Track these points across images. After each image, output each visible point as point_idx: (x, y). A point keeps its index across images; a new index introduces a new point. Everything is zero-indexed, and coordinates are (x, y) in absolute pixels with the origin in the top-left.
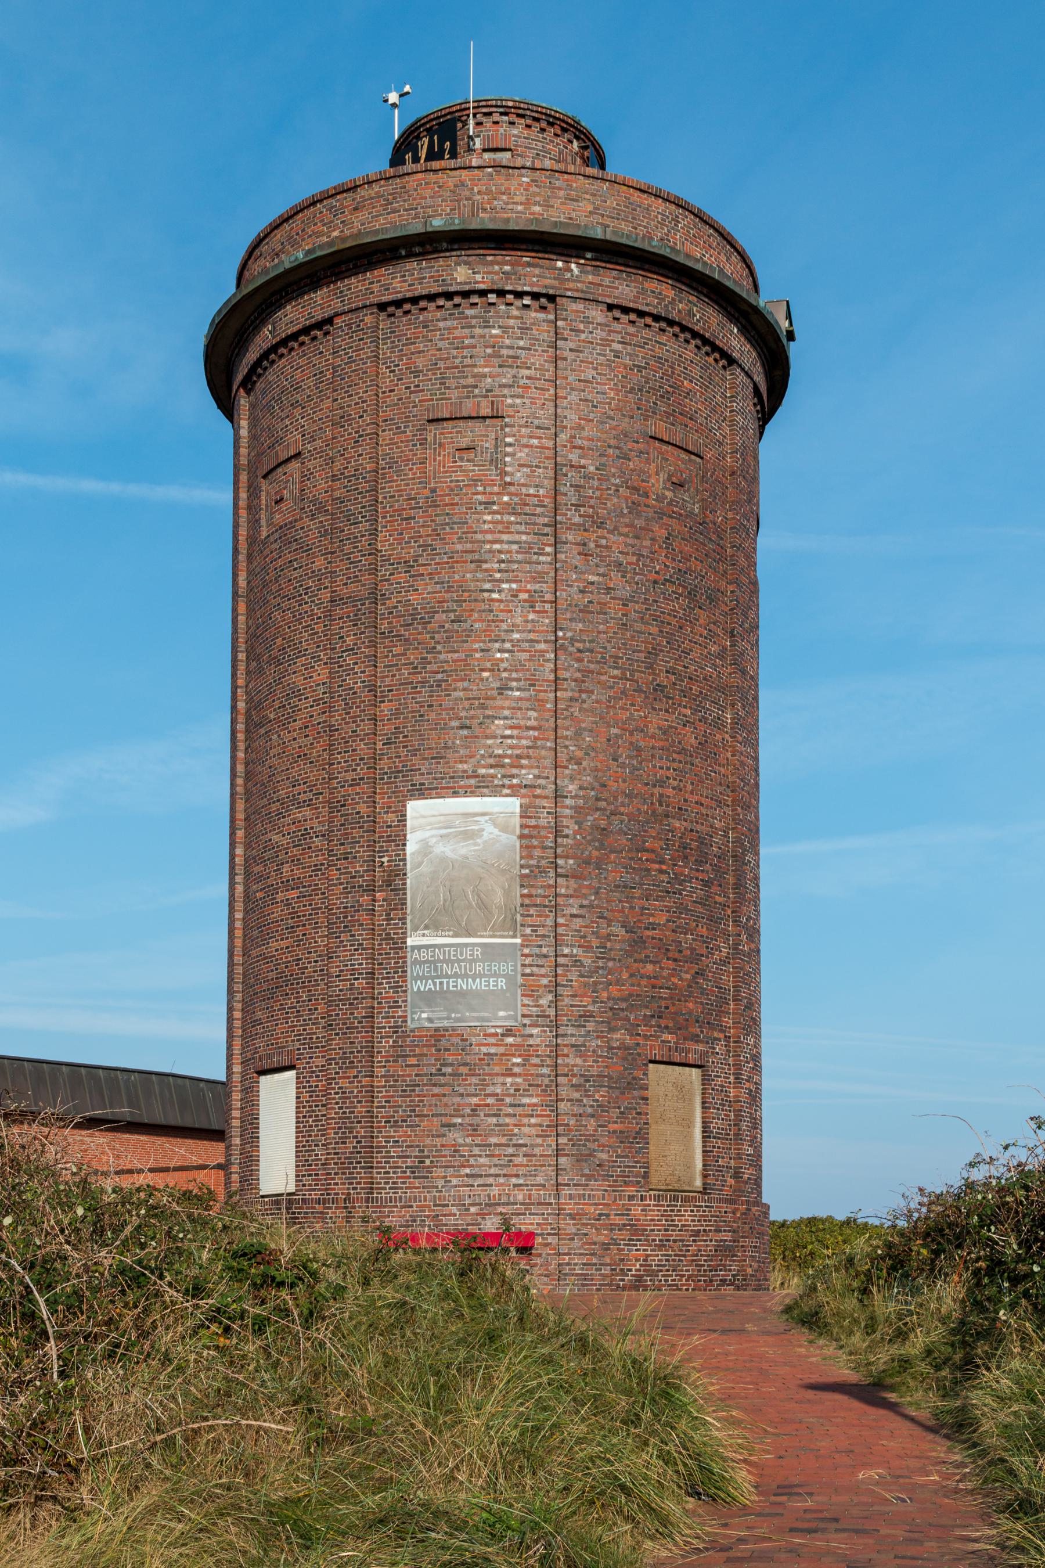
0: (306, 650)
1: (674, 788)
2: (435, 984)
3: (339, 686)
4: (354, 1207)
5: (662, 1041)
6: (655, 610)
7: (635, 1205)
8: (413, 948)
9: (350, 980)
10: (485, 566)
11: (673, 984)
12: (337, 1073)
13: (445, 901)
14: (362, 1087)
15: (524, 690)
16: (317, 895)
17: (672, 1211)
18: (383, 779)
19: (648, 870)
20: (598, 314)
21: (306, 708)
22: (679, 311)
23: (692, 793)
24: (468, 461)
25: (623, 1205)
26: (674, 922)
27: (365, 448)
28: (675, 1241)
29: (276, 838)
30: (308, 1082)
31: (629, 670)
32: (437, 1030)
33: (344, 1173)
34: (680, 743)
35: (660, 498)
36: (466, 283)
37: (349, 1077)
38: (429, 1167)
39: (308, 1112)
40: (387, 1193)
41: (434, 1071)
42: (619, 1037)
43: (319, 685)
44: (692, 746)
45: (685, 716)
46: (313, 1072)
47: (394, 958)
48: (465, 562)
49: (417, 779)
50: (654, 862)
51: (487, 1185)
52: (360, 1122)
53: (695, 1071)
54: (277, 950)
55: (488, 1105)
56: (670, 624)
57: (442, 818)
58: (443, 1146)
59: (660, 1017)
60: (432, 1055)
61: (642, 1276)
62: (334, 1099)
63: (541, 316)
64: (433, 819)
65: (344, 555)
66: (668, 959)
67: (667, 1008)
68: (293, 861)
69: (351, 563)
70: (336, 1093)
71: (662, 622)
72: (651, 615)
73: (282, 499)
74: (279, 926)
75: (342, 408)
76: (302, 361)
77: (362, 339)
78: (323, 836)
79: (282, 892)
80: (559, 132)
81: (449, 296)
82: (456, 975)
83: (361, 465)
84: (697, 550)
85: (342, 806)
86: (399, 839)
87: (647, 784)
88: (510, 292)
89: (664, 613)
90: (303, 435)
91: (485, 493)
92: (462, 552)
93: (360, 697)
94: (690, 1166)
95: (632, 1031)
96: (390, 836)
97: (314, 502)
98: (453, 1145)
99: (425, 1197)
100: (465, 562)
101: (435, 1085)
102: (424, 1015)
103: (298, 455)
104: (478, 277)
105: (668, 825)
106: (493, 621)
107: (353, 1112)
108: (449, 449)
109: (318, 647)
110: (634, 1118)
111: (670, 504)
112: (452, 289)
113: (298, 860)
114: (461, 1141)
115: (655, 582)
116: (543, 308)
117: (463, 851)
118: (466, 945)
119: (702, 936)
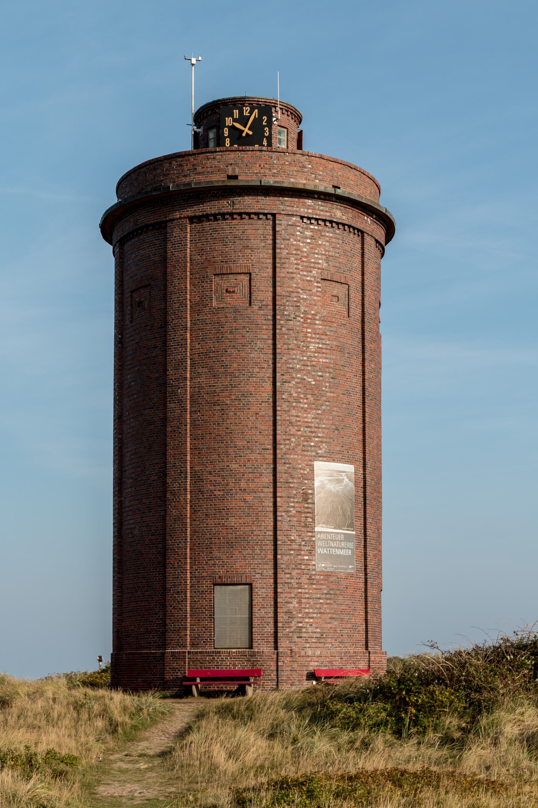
2: (327, 550)
8: (318, 532)
13: (331, 511)
38: (325, 638)
57: (329, 471)
58: (331, 628)
64: (325, 472)
82: (335, 547)
86: (311, 478)
102: (323, 565)
104: (344, 217)
117: (337, 489)
118: (339, 533)
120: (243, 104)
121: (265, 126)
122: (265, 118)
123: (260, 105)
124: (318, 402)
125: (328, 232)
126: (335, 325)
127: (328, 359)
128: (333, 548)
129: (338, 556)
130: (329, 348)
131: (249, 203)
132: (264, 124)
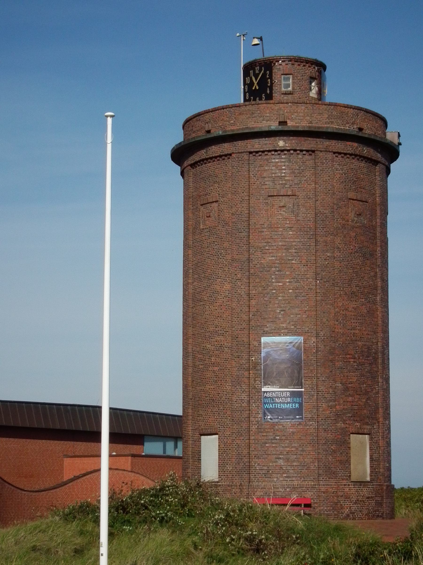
0: (221, 276)
1: (359, 330)
2: (272, 405)
3: (235, 293)
4: (243, 488)
5: (355, 426)
6: (351, 264)
7: (346, 488)
8: (264, 392)
9: (240, 403)
10: (290, 251)
11: (359, 404)
12: (236, 438)
14: (246, 443)
15: (305, 296)
16: (226, 370)
17: (359, 490)
18: (252, 328)
19: (350, 362)
20: (330, 156)
21: (221, 298)
22: (359, 151)
23: (365, 331)
24: (283, 211)
25: (342, 488)
26: (359, 380)
27: (245, 205)
28: (360, 501)
29: (208, 346)
30: (223, 440)
31: (342, 287)
32: (273, 422)
33: (239, 475)
34: (360, 312)
35: (353, 221)
36: (282, 147)
37: (240, 440)
38: (270, 474)
39: (223, 451)
40: (255, 484)
41: (272, 438)
42: (340, 425)
43: (226, 290)
44: (365, 313)
45: (362, 302)
46: (226, 436)
47: (257, 395)
48: (283, 249)
49: (266, 329)
50: (352, 358)
51: (292, 480)
52: (245, 456)
53: (367, 436)
54: (209, 389)
55: (293, 451)
56: (356, 268)
58: (276, 466)
59: (354, 417)
60: (272, 432)
61: (349, 514)
62: (235, 447)
63: (310, 157)
65: (237, 243)
66: (357, 394)
67: (356, 413)
68: (216, 356)
69: (240, 247)
70: (235, 445)
71: (354, 268)
72: (350, 266)
73: (209, 216)
74: (210, 380)
75: (235, 188)
76: (219, 166)
77: (243, 164)
78: (229, 348)
79: (212, 367)
80: (310, 65)
81: (276, 151)
83: (243, 211)
84: (366, 238)
85: (237, 338)
87: (349, 329)
88: (298, 150)
89: (354, 264)
90: (219, 195)
91: (289, 224)
92: (281, 245)
93: (243, 297)
94: (365, 472)
95: (344, 422)
96: (255, 350)
97: (224, 221)
98: (280, 466)
99: (270, 485)
100: (283, 249)
101: (273, 443)
102: (269, 417)
103: (216, 201)
104: (287, 145)
105: (357, 344)
106: (293, 271)
107: (242, 453)
108: (276, 207)
109: (226, 276)
110: (345, 455)
111: (356, 223)
112: (277, 149)
113: (218, 356)
114: (282, 464)
115: (351, 253)
116: (311, 155)
119: (369, 384)
120: (255, 65)
121: (268, 78)
122: (268, 72)
123: (266, 62)
124: (265, 291)
125: (274, 159)
126: (281, 229)
127: (274, 257)
128: (278, 403)
129: (282, 409)
130: (275, 248)
131: (215, 150)
132: (268, 77)
